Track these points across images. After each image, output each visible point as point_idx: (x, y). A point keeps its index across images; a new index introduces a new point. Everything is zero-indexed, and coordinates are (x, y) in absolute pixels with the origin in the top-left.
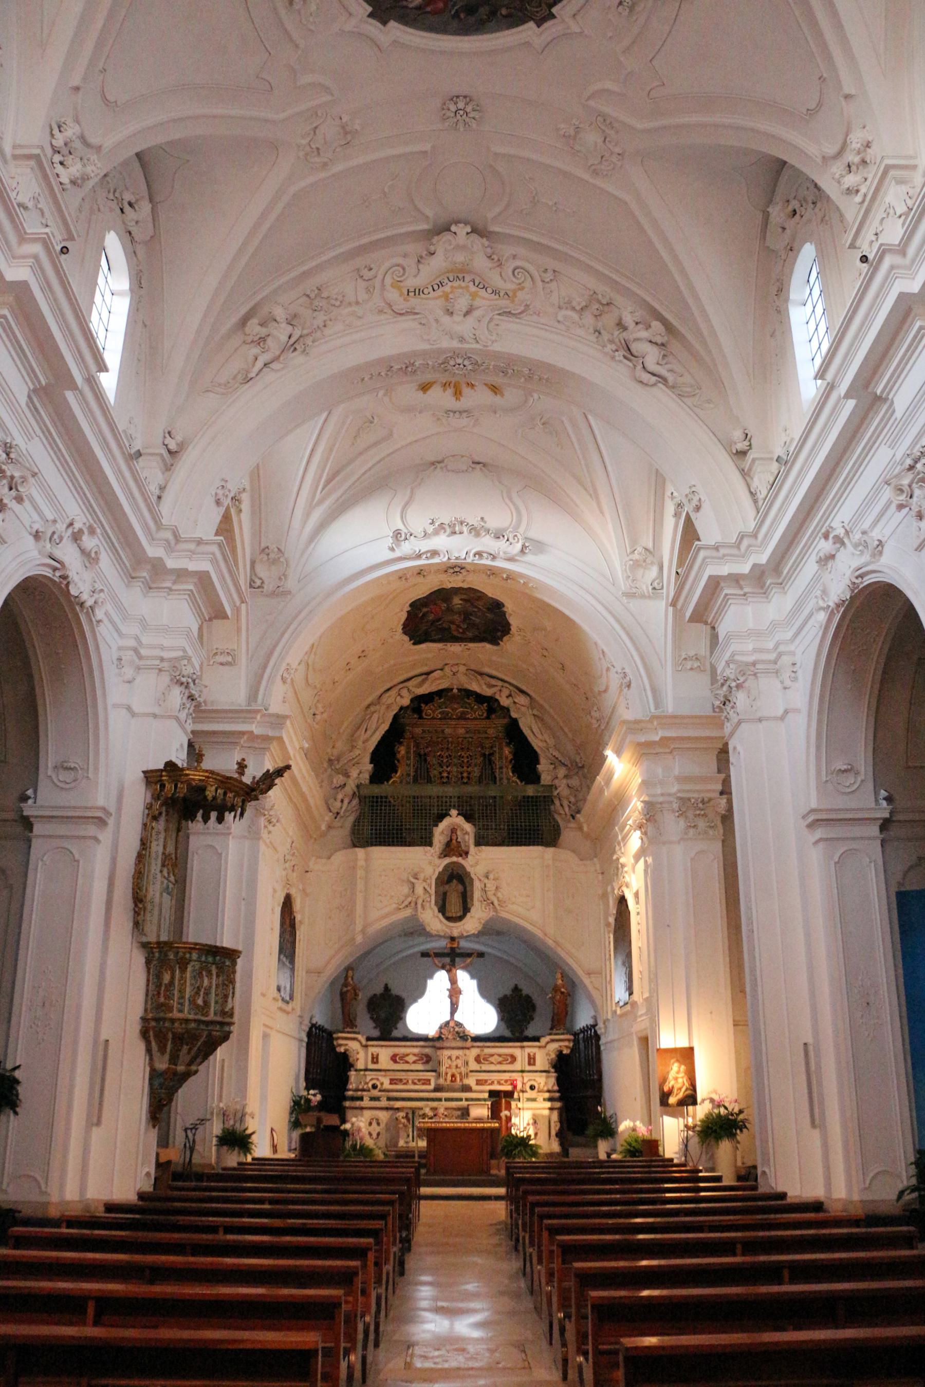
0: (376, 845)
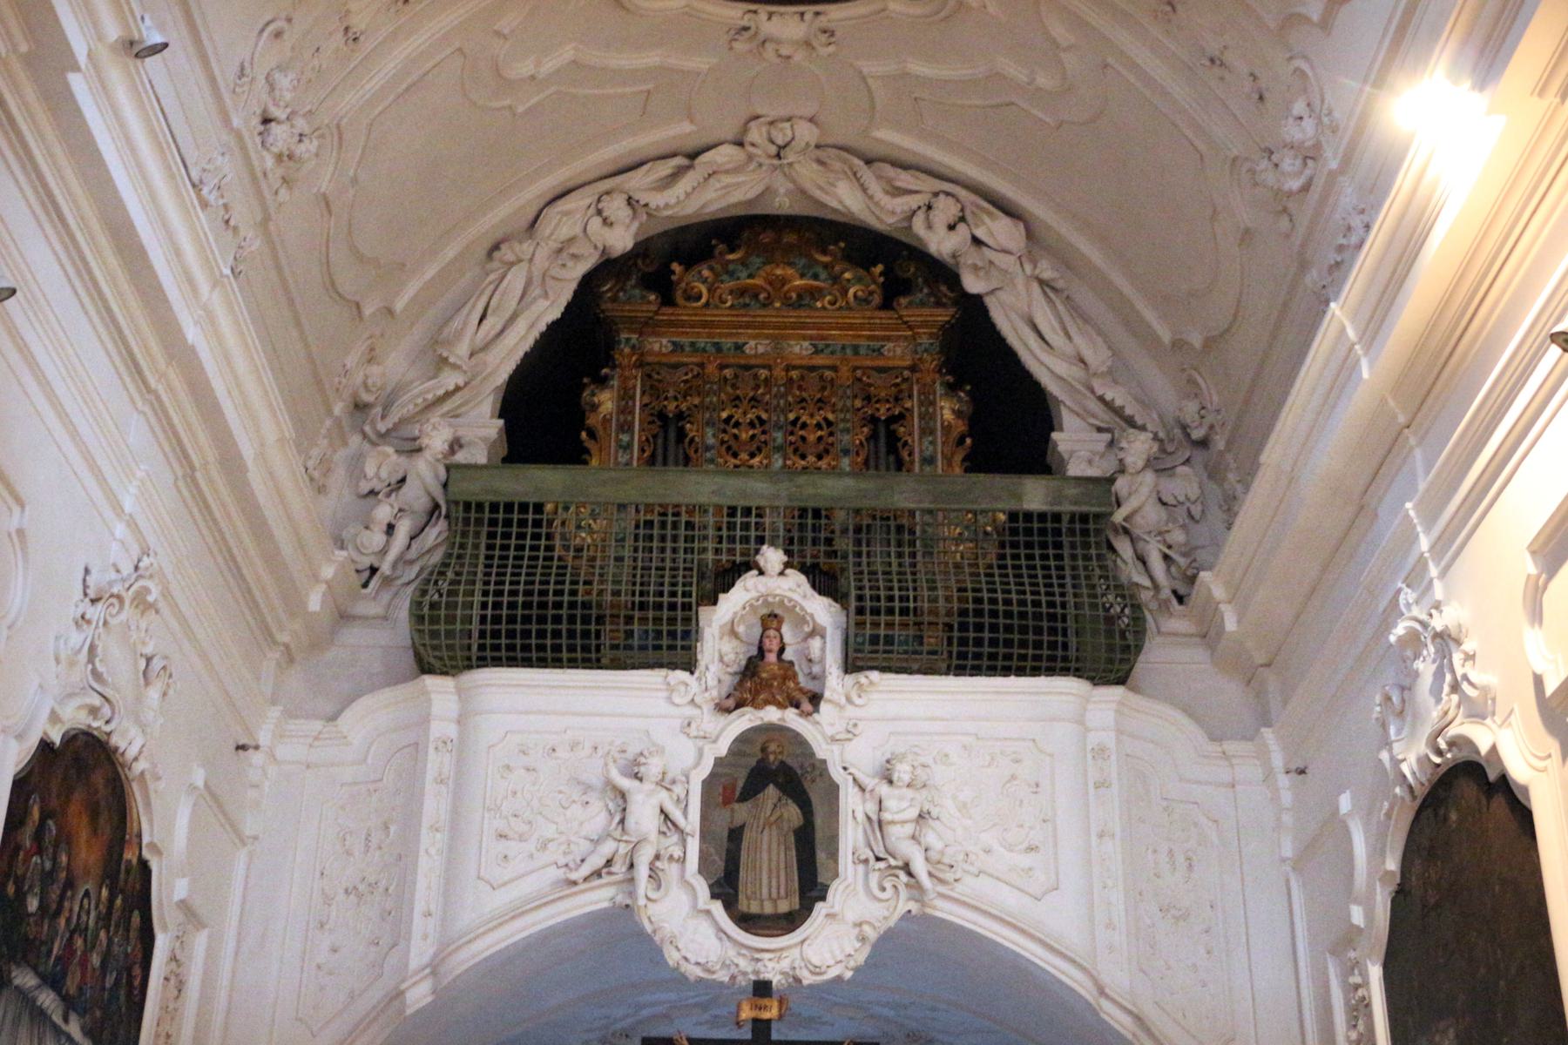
0: (497, 662)
